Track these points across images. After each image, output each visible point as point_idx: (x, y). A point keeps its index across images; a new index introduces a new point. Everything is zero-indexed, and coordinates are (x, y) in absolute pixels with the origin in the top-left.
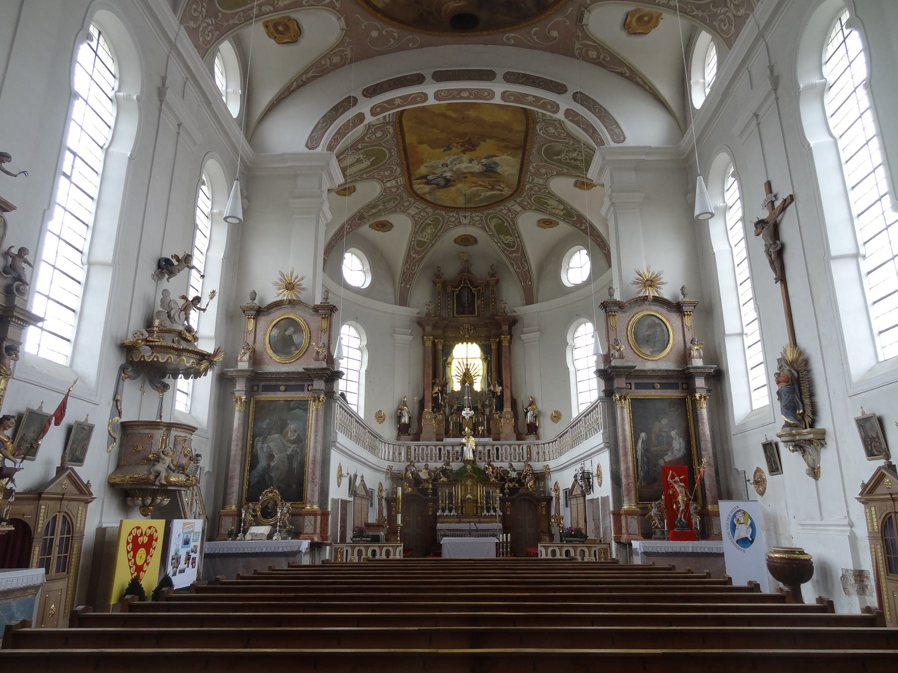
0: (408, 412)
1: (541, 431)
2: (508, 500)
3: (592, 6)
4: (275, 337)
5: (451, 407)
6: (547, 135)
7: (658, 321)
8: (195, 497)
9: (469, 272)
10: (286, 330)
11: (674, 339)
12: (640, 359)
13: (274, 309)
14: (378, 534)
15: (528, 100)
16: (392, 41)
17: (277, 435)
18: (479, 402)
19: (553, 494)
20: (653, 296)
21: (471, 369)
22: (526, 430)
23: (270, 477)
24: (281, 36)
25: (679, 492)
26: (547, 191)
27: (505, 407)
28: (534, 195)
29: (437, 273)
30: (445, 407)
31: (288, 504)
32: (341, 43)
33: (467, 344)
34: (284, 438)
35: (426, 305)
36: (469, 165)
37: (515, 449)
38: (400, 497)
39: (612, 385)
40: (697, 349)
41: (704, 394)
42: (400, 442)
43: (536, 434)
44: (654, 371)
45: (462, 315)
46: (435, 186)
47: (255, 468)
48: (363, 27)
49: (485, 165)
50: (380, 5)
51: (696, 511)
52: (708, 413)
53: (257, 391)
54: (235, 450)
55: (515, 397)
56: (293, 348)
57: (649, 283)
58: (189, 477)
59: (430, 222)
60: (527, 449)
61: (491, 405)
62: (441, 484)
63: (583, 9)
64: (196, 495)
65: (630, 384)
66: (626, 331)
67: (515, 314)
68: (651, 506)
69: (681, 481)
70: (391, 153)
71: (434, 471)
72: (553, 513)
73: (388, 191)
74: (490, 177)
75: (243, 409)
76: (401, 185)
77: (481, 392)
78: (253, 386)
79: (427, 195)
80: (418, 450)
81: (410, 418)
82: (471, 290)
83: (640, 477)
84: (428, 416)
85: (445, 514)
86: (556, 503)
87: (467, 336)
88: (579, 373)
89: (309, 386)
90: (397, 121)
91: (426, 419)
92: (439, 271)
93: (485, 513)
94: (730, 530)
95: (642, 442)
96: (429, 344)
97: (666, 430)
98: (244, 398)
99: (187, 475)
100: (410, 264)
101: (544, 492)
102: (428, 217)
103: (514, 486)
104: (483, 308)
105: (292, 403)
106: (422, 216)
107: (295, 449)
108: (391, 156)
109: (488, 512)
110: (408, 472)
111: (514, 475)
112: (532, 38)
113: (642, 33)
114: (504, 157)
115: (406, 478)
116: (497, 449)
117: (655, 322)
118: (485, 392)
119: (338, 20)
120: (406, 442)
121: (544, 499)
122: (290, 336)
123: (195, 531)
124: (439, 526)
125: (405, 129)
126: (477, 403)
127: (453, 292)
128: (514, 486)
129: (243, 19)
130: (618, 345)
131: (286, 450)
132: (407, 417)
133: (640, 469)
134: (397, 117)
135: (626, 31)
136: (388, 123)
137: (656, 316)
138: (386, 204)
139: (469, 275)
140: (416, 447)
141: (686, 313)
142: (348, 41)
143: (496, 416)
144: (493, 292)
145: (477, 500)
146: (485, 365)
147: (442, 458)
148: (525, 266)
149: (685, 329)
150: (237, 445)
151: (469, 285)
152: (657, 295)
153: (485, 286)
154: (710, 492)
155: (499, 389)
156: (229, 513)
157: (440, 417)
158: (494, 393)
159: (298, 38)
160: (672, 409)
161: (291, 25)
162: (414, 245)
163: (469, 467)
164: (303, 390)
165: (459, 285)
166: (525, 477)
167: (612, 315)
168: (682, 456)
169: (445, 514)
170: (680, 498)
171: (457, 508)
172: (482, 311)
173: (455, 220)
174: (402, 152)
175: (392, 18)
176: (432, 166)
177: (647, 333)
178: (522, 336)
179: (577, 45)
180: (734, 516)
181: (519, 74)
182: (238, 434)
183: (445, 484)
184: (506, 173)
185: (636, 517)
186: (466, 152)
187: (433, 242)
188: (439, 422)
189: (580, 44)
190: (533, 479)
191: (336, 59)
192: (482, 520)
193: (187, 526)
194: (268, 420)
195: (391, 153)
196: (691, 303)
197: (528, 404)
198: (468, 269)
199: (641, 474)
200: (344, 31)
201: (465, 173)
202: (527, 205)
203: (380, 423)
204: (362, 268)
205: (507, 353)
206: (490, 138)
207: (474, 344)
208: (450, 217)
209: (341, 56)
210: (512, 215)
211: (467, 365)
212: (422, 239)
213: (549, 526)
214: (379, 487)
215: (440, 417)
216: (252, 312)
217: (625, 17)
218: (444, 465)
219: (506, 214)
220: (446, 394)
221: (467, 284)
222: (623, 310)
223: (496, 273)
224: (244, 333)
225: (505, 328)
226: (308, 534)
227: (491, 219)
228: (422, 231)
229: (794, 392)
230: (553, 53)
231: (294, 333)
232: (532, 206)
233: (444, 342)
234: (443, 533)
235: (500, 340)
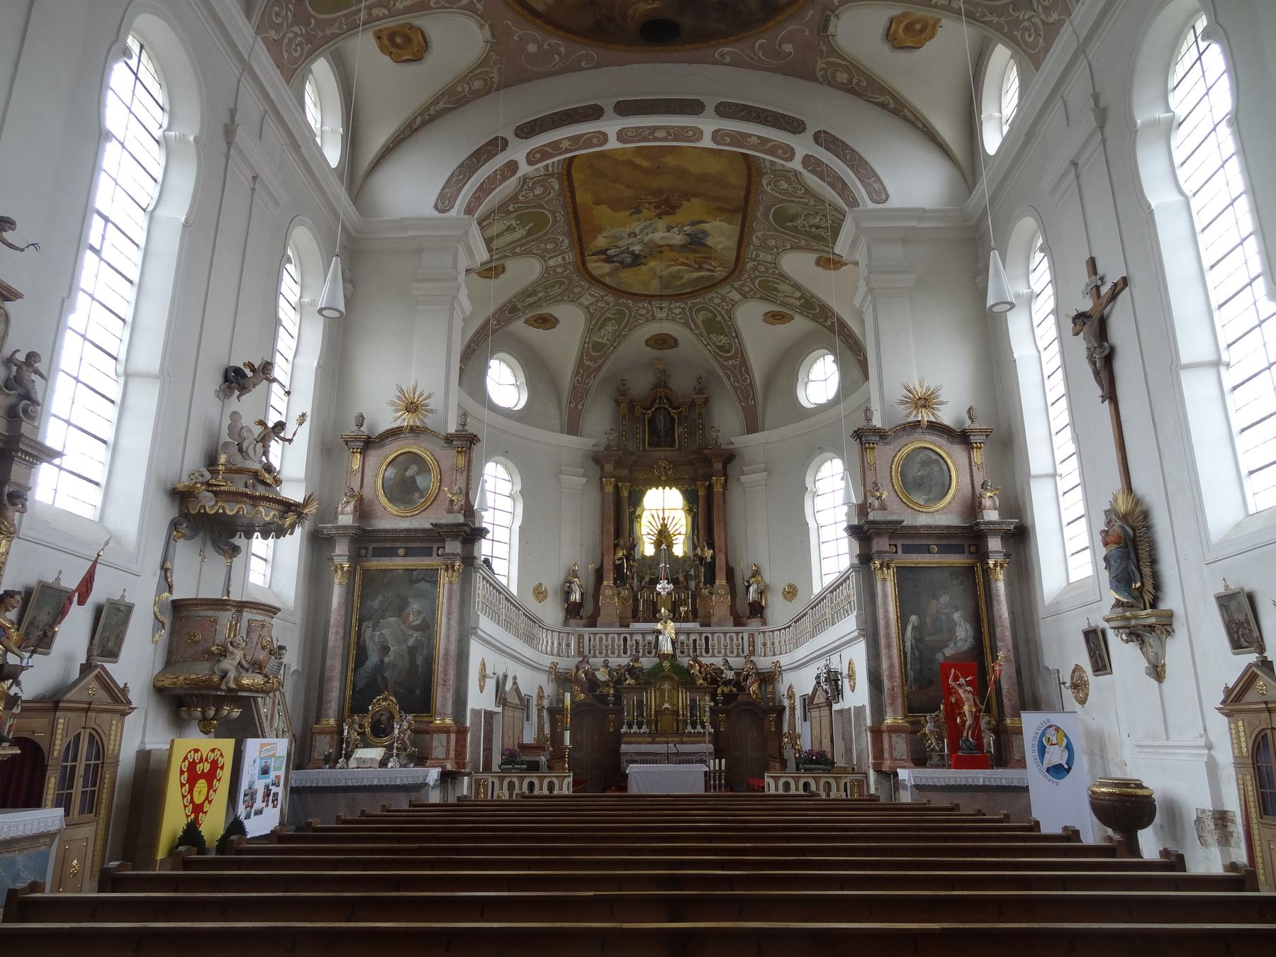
0: (580, 586)
1: (769, 613)
2: (722, 711)
3: (841, 8)
4: (391, 479)
5: (641, 579)
6: (777, 192)
7: (934, 457)
8: (277, 707)
9: (666, 386)
10: (406, 470)
11: (957, 482)
12: (909, 510)
13: (390, 439)
14: (537, 759)
15: (750, 142)
16: (557, 58)
17: (394, 619)
18: (681, 571)
19: (786, 703)
20: (928, 422)
21: (669, 524)
22: (747, 612)
23: (384, 678)
24: (399, 51)
25: (965, 700)
26: (777, 272)
27: (717, 578)
28: (758, 277)
29: (622, 388)
30: (633, 579)
31: (410, 717)
32: (484, 62)
33: (664, 489)
34: (404, 622)
35: (606, 433)
36: (667, 234)
37: (731, 639)
38: (569, 707)
39: (870, 547)
40: (990, 497)
41: (1000, 561)
42: (568, 629)
43: (762, 617)
44: (929, 527)
45: (657, 449)
46: (618, 264)
47: (363, 666)
48: (516, 38)
49: (689, 235)
50: (540, 7)
51: (988, 727)
52: (1006, 588)
53: (366, 556)
54: (333, 639)
55: (732, 564)
56: (417, 495)
57: (923, 402)
58: (269, 679)
59: (611, 316)
60: (749, 638)
61: (697, 576)
62: (626, 688)
63: (828, 13)
64: (279, 704)
65: (896, 546)
66: (889, 471)
67: (732, 447)
68: (925, 720)
69: (968, 683)
70: (555, 218)
71: (616, 670)
72: (785, 729)
73: (551, 272)
74: (696, 251)
75: (345, 581)
76: (570, 263)
77: (683, 557)
78: (359, 549)
79: (607, 277)
80: (595, 640)
81: (582, 594)
82: (669, 412)
83: (909, 679)
84: (608, 592)
85: (632, 731)
86: (790, 715)
87: (663, 478)
88: (822, 531)
89: (438, 548)
90: (565, 172)
91: (605, 595)
92: (624, 385)
93: (689, 729)
94: (1037, 754)
95: (913, 628)
96: (609, 489)
97: (947, 611)
98: (346, 565)
99: (266, 676)
100: (583, 375)
101: (773, 699)
102: (608, 309)
103: (731, 691)
104: (686, 438)
105: (415, 573)
106: (600, 307)
107: (419, 638)
108: (555, 222)
109: (694, 727)
110: (580, 672)
111: (730, 675)
112: (756, 54)
113: (912, 48)
114: (717, 223)
115: (576, 680)
116: (707, 638)
117: (930, 457)
118: (689, 557)
119: (480, 29)
120: (577, 629)
121: (773, 710)
122: (413, 478)
123: (277, 755)
124: (624, 748)
125: (576, 184)
126: (678, 573)
127: (644, 415)
128: (731, 691)
129: (345, 27)
130: (878, 490)
131: (406, 640)
132: (578, 593)
133: (909, 666)
134: (565, 167)
135: (890, 44)
136: (551, 175)
137: (932, 450)
138: (549, 290)
139: (666, 390)
140: (592, 636)
141: (975, 445)
142: (494, 58)
143: (705, 592)
144: (700, 415)
145: (678, 712)
146: (690, 519)
147: (629, 651)
148: (746, 378)
149: (973, 467)
150: (337, 633)
151: (667, 406)
152: (933, 420)
153: (689, 407)
154: (1009, 700)
155: (708, 553)
156: (326, 729)
157: (625, 593)
158: (702, 559)
159: (424, 54)
160: (955, 582)
161: (413, 36)
162: (588, 348)
163: (666, 664)
164: (431, 555)
165: (652, 405)
166: (746, 678)
167: (870, 448)
168: (970, 649)
169: (632, 731)
170: (966, 708)
171: (649, 723)
172: (685, 442)
173: (647, 313)
174: (572, 216)
175: (557, 26)
176: (614, 236)
177: (919, 474)
178: (741, 477)
179: (820, 64)
180: (1043, 734)
181: (737, 105)
182: (339, 618)
183: (633, 688)
184: (720, 247)
185: (903, 735)
186: (663, 216)
187: (616, 344)
188: (623, 601)
189: (824, 63)
190: (757, 681)
191: (478, 84)
192: (684, 739)
193: (265, 748)
194: (380, 598)
195: (555, 218)
196: (981, 431)
197: (750, 575)
198: (665, 382)
199: (911, 674)
200: (489, 45)
201: (660, 246)
202: (748, 292)
203: (540, 602)
204: (514, 382)
205: (721, 503)
206: (697, 196)
207: (674, 489)
208: (640, 308)
209: (485, 80)
210: (727, 306)
211: (664, 519)
212: (600, 340)
213: (781, 748)
214: (539, 692)
215: (625, 593)
216: (358, 444)
217: (888, 23)
218: (631, 661)
219: (718, 305)
220: (634, 560)
221: (664, 404)
222: (886, 441)
223: (704, 388)
224: (347, 473)
225: (718, 466)
226: (437, 759)
227: (698, 311)
228: (600, 328)
229: (1128, 558)
230: (785, 75)
231: (418, 473)
232: (755, 293)
233: (631, 487)
234: (629, 758)
235: (710, 484)
